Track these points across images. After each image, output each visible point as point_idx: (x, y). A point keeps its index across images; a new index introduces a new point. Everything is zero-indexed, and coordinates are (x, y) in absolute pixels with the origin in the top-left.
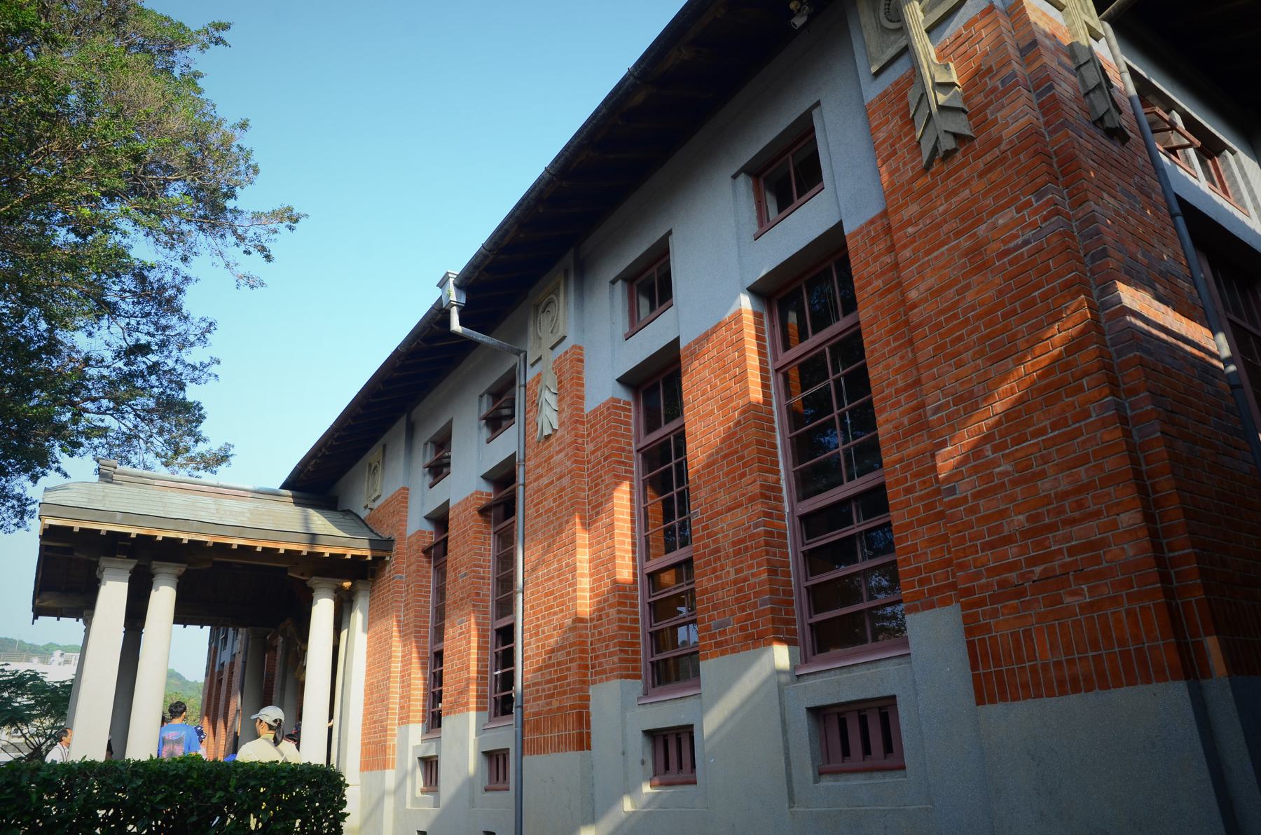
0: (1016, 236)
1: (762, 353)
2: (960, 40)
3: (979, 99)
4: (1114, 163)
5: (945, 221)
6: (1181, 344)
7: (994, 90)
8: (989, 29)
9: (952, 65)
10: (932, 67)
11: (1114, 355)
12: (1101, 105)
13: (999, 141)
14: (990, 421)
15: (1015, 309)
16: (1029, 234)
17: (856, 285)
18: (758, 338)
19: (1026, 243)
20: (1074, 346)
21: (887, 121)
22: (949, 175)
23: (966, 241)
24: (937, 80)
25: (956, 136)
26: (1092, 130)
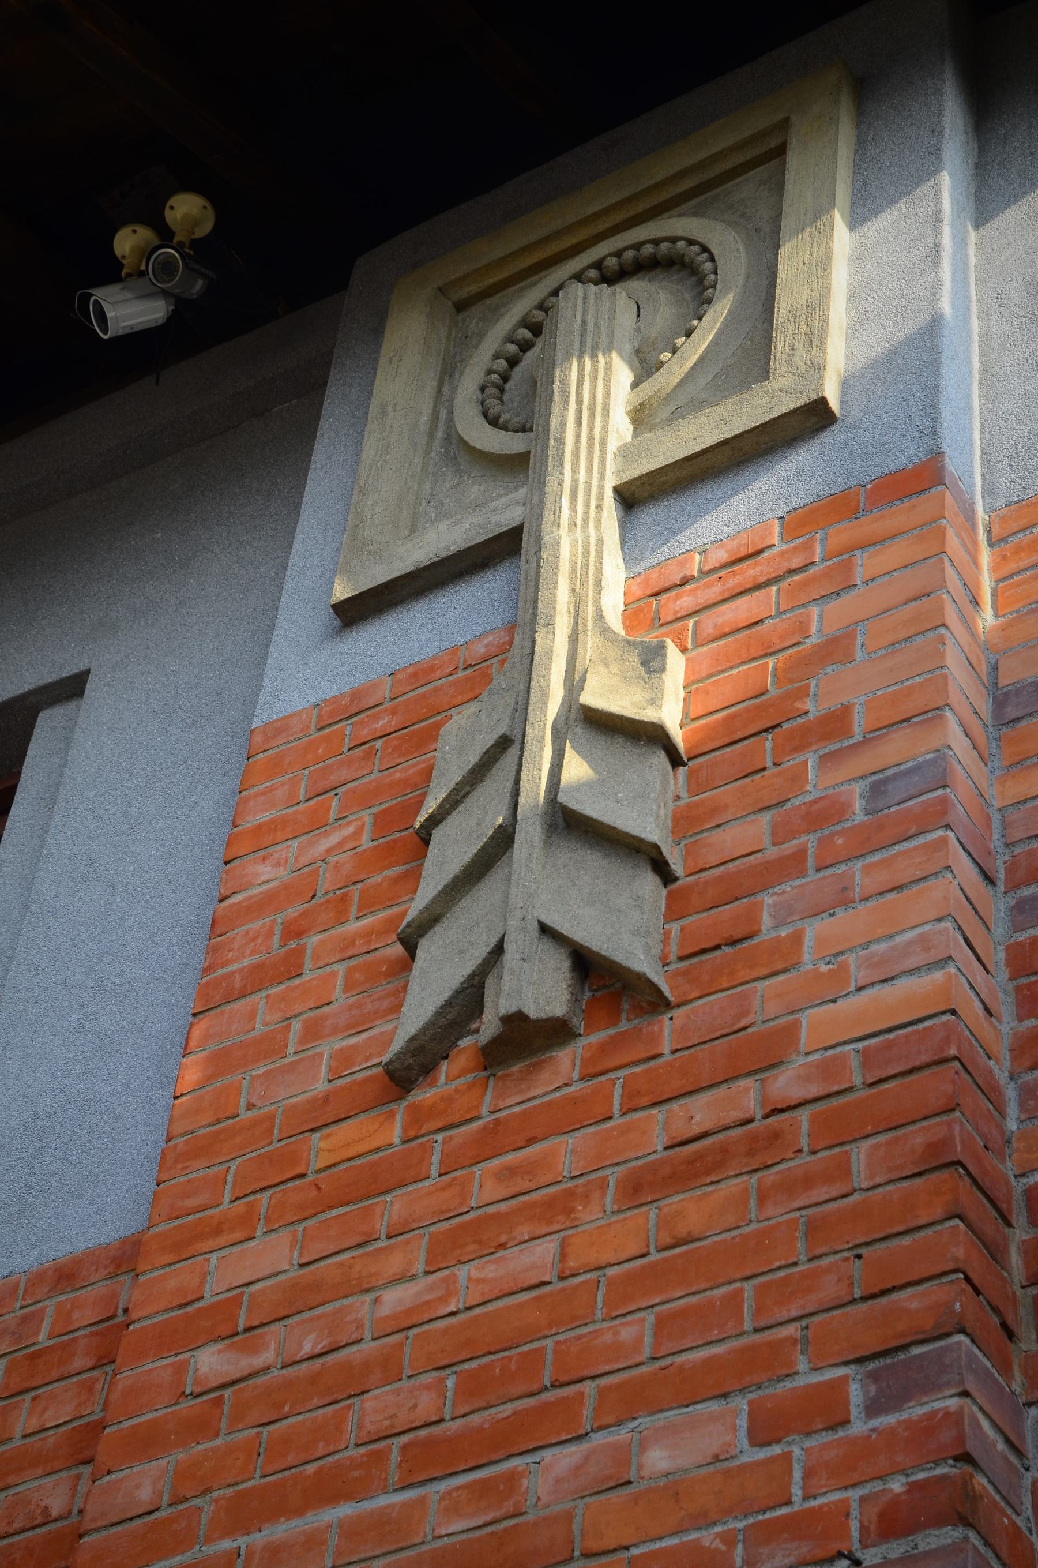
2: (750, 572)
3: (746, 835)
5: (389, 1368)
7: (825, 814)
9: (676, 662)
10: (591, 644)
13: (767, 1054)
21: (317, 824)
22: (492, 1141)
23: (452, 1507)
24: (592, 697)
25: (586, 966)
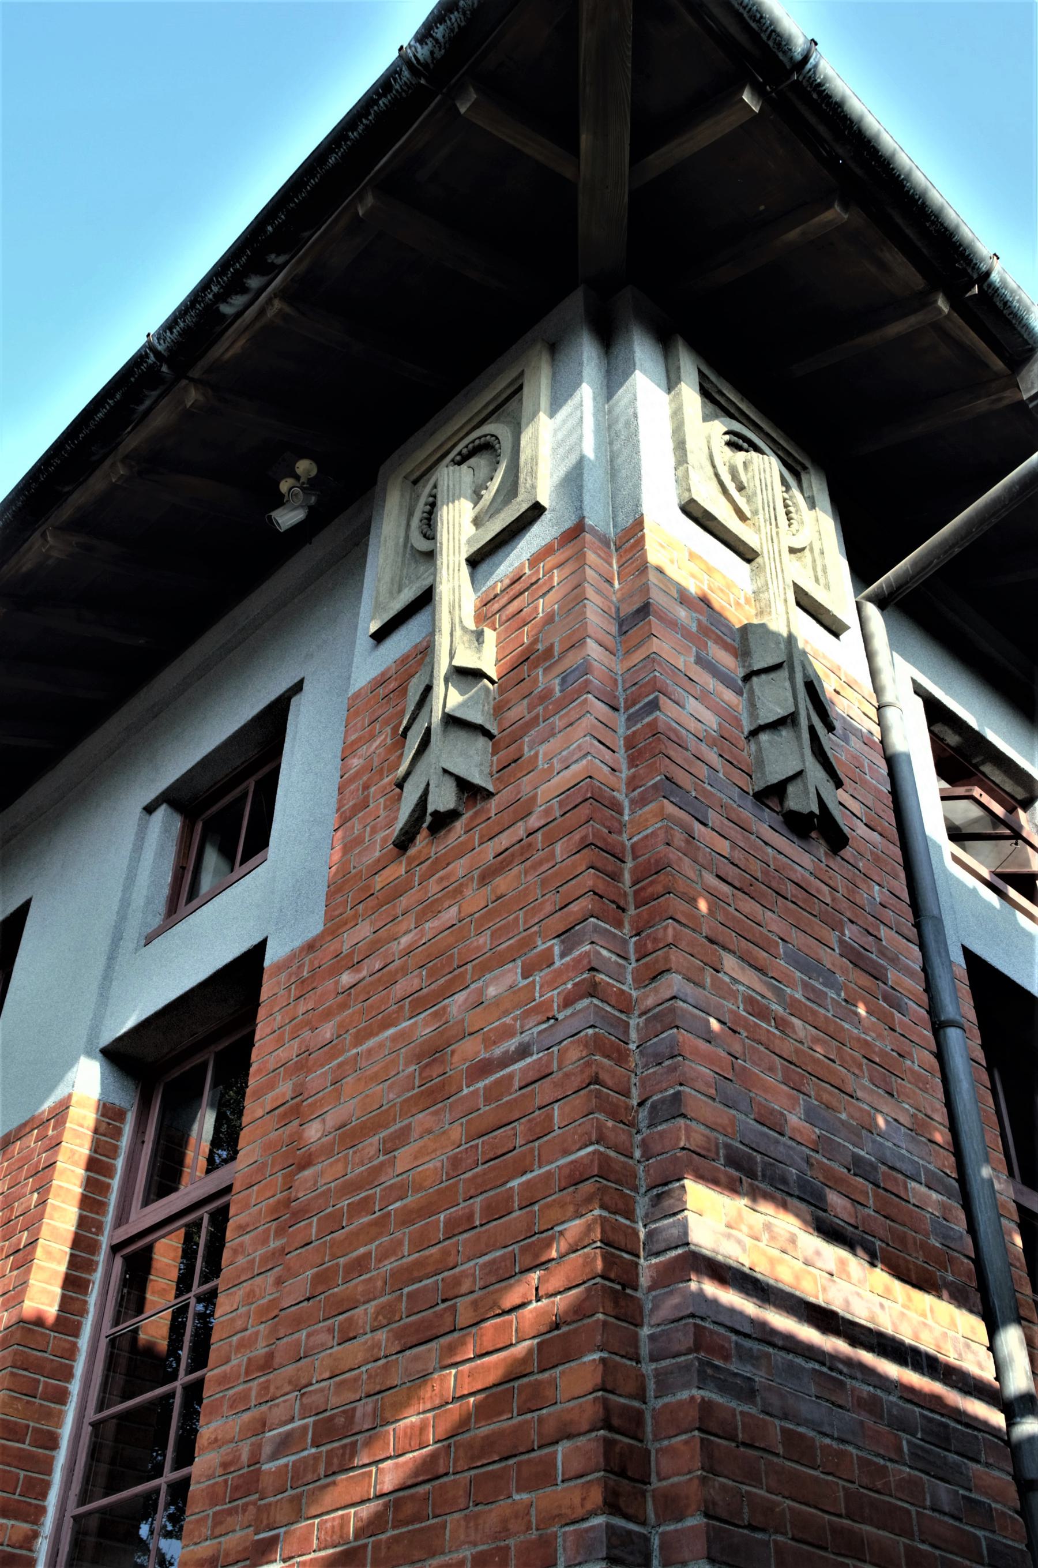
0: (508, 1032)
1: (91, 1201)
2: (518, 587)
3: (519, 711)
4: (790, 889)
5: (404, 971)
6: (867, 1357)
8: (567, 569)
10: (458, 632)
11: (651, 1386)
12: (783, 756)
14: (365, 1511)
15: (470, 1217)
16: (534, 1030)
17: (252, 1082)
18: (92, 1165)
19: (523, 1051)
20: (556, 1343)
21: (372, 737)
23: (426, 1024)
25: (464, 786)
26: (747, 812)
